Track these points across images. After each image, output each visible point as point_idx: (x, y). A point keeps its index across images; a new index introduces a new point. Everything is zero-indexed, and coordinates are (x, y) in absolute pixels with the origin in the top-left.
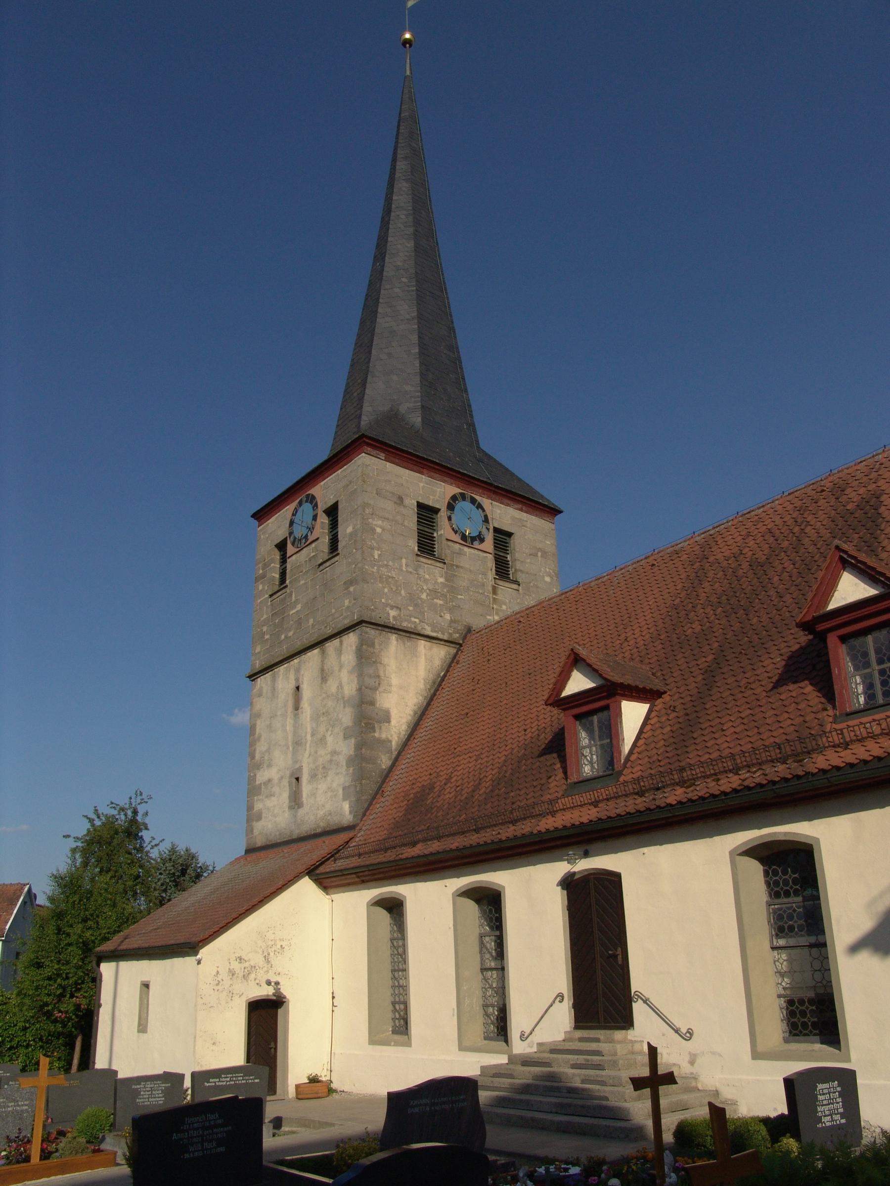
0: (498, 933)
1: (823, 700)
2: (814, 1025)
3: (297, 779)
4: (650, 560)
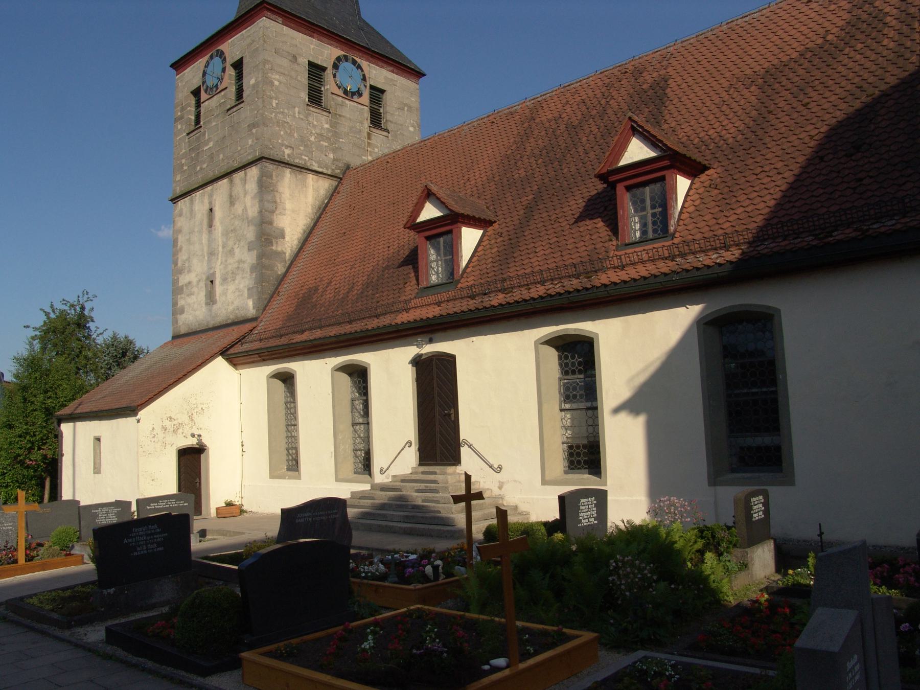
0: (365, 398)
1: (610, 233)
2: (585, 462)
3: (212, 282)
4: (490, 118)
